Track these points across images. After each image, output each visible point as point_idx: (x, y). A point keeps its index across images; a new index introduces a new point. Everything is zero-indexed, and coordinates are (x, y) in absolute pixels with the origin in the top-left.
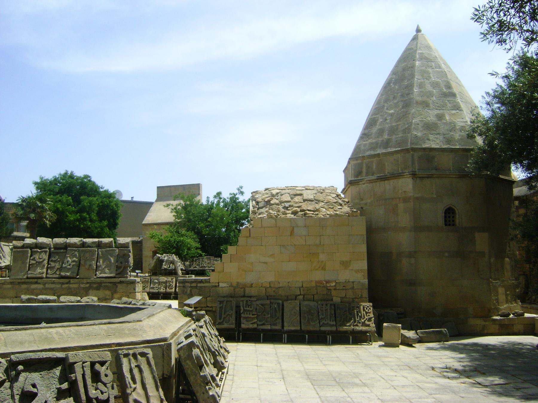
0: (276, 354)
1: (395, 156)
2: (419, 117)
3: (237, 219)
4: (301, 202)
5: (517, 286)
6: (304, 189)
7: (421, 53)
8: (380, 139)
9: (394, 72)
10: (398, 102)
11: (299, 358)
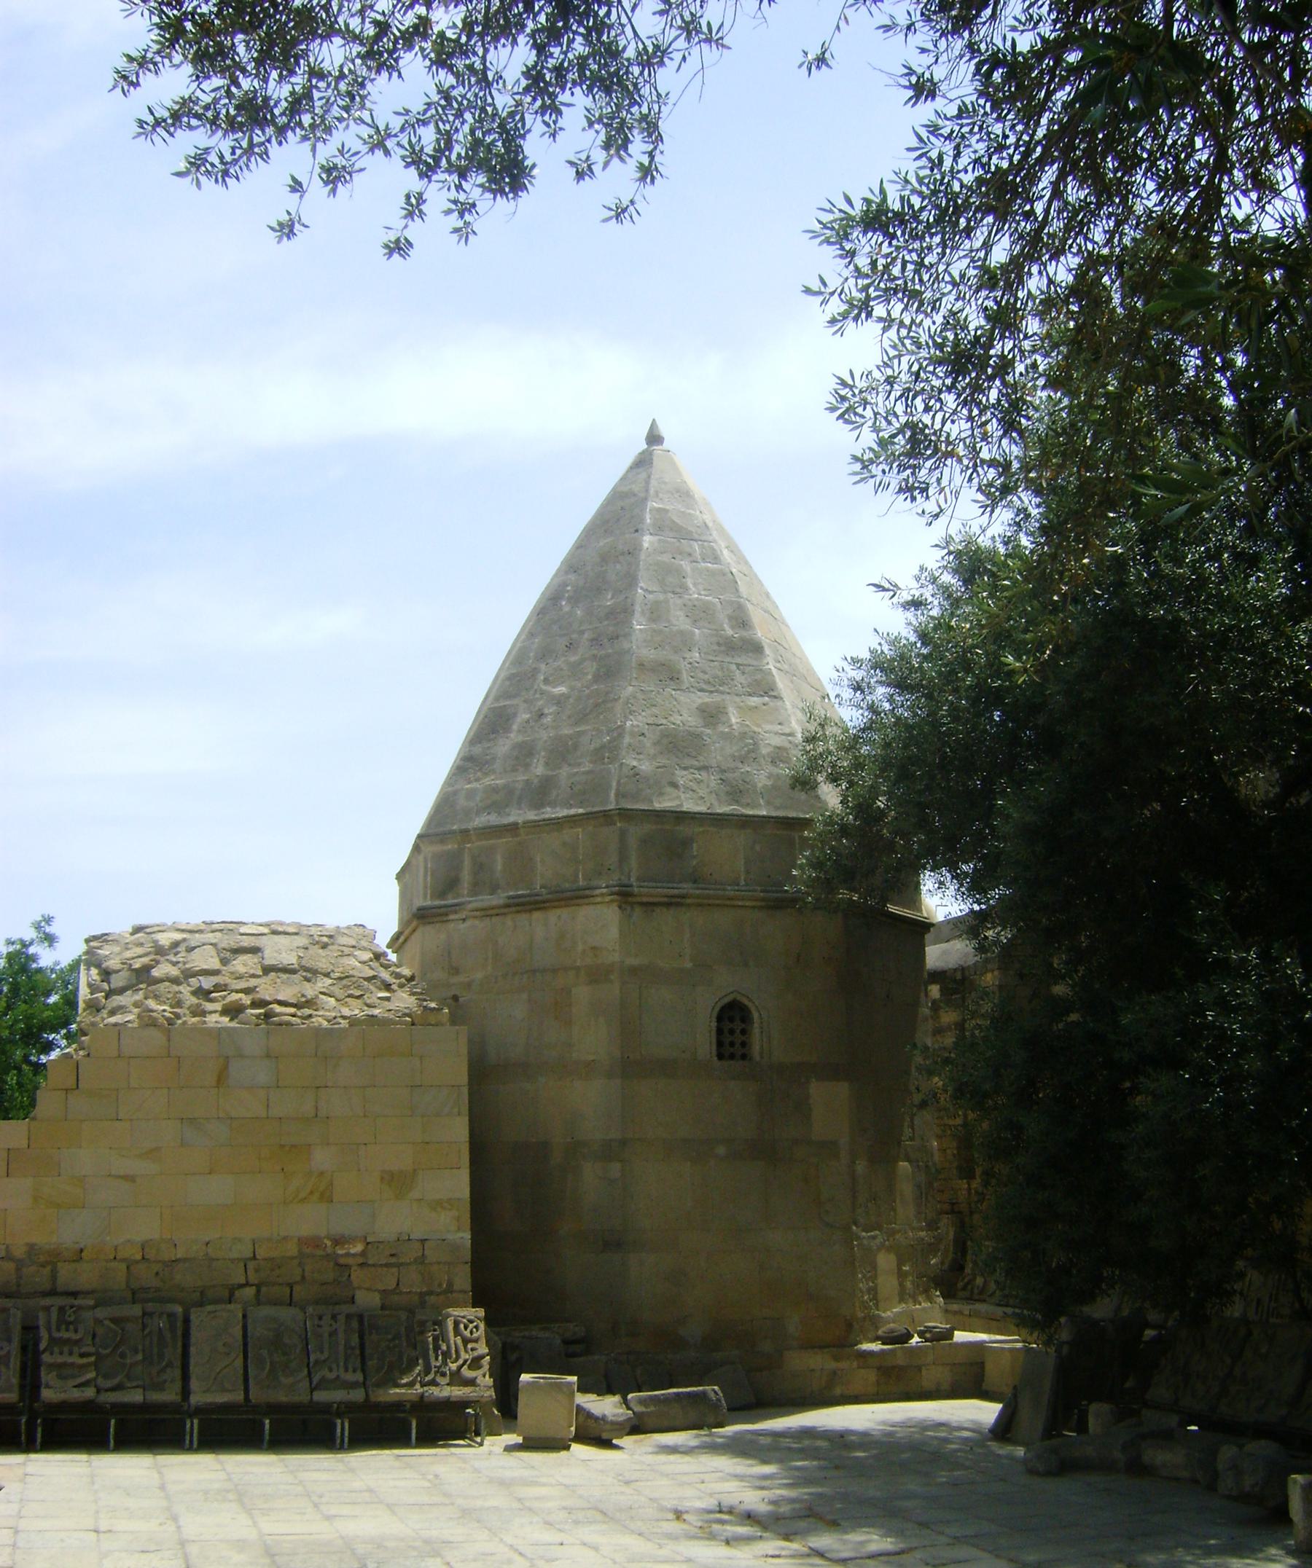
0: (162, 1487)
1: (568, 834)
2: (645, 713)
3: (29, 1027)
4: (253, 976)
5: (932, 1248)
6: (266, 930)
7: (659, 510)
8: (521, 777)
9: (572, 565)
10: (582, 661)
11: (240, 1496)
